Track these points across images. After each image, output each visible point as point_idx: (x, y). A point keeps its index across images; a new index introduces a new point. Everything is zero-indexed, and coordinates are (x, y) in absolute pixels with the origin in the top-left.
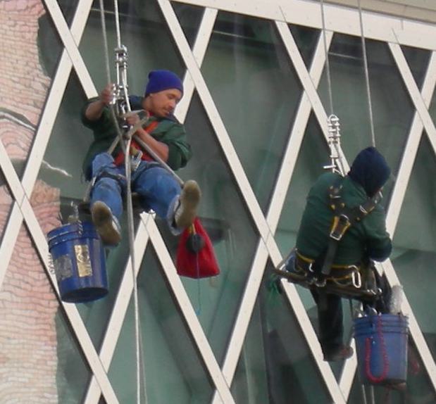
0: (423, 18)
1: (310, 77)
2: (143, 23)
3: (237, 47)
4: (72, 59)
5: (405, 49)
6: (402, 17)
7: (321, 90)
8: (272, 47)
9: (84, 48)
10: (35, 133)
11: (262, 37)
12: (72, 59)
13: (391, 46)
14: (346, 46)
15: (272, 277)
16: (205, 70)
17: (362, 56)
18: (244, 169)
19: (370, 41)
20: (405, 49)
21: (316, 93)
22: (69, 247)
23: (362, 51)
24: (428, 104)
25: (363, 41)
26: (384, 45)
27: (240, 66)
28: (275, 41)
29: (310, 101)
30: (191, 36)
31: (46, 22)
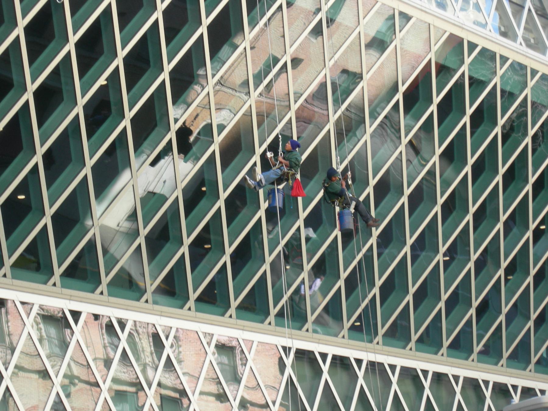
0: (258, 331)
1: (361, 374)
2: (310, 358)
3: (338, 365)
4: (289, 370)
5: (320, 353)
6: (451, 366)
7: (293, 366)
8: (349, 365)
9: (364, 378)
10: (40, 357)
11: (345, 362)
12: (289, 370)
13: (508, 385)
14: (372, 364)
15: (139, 387)
16: (329, 372)
17: (376, 367)
18: (407, 407)
19: (378, 363)
20: (320, 353)
21: (396, 384)
22: (246, 405)
23: (376, 365)
24: (460, 391)
25: (376, 363)
26: (382, 364)
27: (339, 370)
28: (349, 363)
29: (361, 381)
30: (393, 374)
31: (281, 359)
